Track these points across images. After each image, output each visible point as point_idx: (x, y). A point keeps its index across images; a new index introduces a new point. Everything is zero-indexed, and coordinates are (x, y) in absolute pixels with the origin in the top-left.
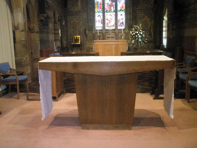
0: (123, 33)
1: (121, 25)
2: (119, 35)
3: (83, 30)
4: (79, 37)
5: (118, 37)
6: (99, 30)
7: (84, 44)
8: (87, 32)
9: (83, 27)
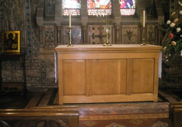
0: (70, 26)
1: (127, 5)
2: (123, 30)
3: (28, 14)
4: (17, 35)
5: (121, 35)
6: (72, 17)
7: (30, 52)
8: (40, 21)
9: (28, 8)
